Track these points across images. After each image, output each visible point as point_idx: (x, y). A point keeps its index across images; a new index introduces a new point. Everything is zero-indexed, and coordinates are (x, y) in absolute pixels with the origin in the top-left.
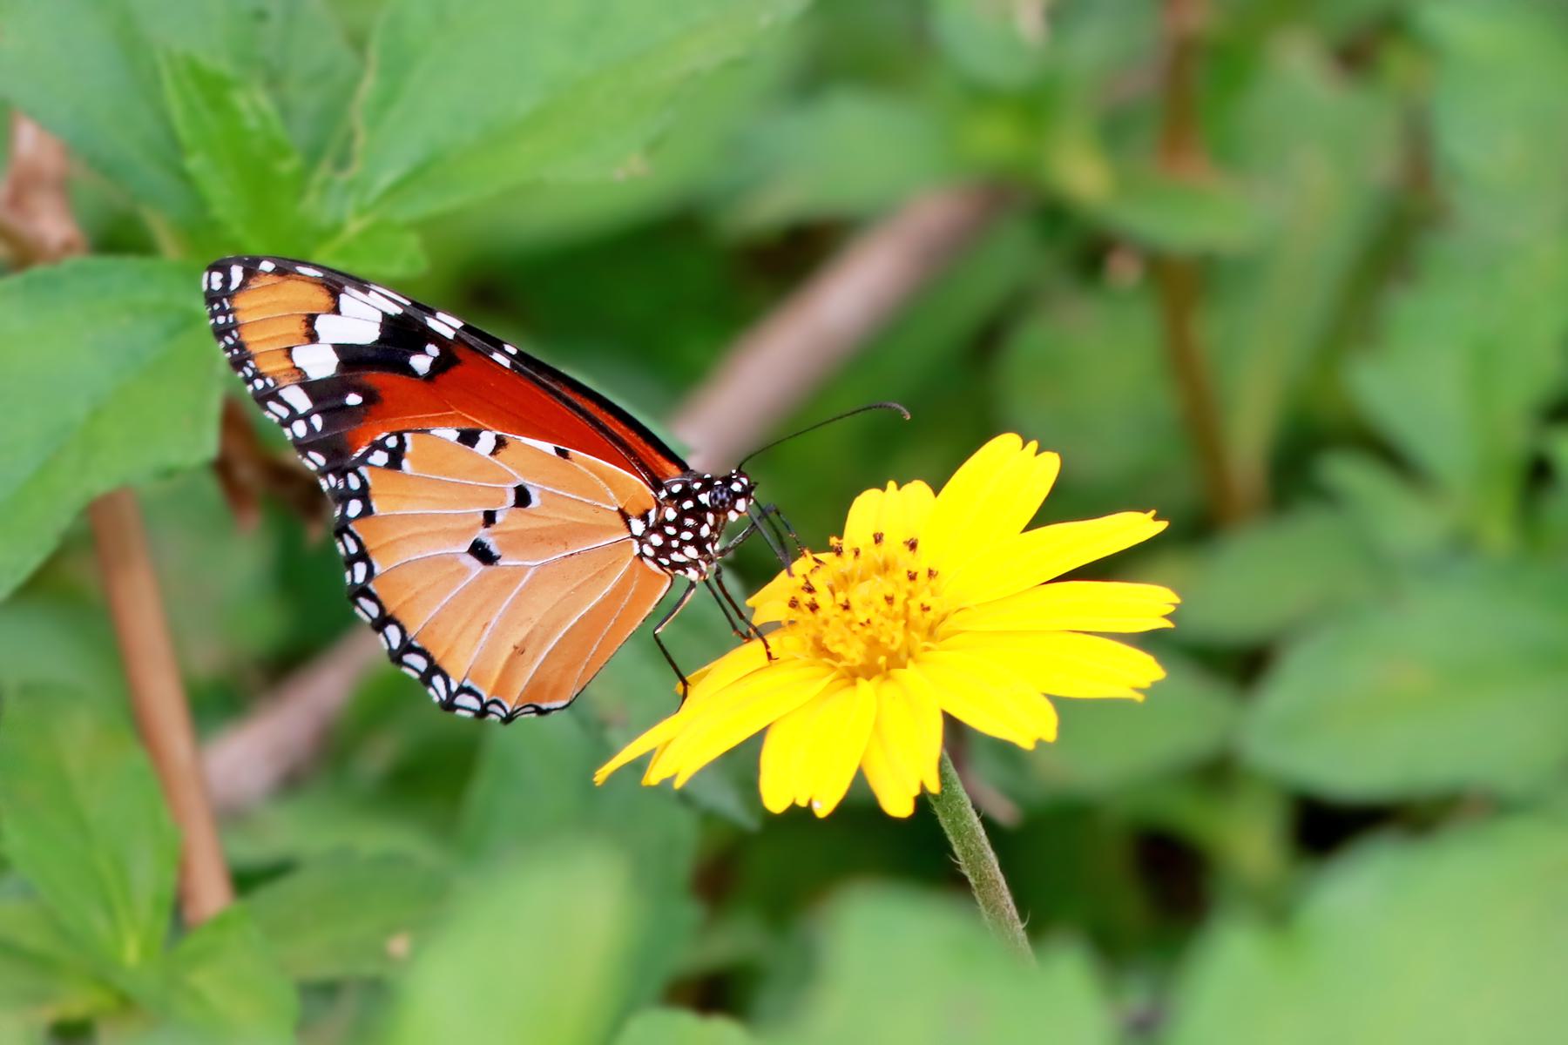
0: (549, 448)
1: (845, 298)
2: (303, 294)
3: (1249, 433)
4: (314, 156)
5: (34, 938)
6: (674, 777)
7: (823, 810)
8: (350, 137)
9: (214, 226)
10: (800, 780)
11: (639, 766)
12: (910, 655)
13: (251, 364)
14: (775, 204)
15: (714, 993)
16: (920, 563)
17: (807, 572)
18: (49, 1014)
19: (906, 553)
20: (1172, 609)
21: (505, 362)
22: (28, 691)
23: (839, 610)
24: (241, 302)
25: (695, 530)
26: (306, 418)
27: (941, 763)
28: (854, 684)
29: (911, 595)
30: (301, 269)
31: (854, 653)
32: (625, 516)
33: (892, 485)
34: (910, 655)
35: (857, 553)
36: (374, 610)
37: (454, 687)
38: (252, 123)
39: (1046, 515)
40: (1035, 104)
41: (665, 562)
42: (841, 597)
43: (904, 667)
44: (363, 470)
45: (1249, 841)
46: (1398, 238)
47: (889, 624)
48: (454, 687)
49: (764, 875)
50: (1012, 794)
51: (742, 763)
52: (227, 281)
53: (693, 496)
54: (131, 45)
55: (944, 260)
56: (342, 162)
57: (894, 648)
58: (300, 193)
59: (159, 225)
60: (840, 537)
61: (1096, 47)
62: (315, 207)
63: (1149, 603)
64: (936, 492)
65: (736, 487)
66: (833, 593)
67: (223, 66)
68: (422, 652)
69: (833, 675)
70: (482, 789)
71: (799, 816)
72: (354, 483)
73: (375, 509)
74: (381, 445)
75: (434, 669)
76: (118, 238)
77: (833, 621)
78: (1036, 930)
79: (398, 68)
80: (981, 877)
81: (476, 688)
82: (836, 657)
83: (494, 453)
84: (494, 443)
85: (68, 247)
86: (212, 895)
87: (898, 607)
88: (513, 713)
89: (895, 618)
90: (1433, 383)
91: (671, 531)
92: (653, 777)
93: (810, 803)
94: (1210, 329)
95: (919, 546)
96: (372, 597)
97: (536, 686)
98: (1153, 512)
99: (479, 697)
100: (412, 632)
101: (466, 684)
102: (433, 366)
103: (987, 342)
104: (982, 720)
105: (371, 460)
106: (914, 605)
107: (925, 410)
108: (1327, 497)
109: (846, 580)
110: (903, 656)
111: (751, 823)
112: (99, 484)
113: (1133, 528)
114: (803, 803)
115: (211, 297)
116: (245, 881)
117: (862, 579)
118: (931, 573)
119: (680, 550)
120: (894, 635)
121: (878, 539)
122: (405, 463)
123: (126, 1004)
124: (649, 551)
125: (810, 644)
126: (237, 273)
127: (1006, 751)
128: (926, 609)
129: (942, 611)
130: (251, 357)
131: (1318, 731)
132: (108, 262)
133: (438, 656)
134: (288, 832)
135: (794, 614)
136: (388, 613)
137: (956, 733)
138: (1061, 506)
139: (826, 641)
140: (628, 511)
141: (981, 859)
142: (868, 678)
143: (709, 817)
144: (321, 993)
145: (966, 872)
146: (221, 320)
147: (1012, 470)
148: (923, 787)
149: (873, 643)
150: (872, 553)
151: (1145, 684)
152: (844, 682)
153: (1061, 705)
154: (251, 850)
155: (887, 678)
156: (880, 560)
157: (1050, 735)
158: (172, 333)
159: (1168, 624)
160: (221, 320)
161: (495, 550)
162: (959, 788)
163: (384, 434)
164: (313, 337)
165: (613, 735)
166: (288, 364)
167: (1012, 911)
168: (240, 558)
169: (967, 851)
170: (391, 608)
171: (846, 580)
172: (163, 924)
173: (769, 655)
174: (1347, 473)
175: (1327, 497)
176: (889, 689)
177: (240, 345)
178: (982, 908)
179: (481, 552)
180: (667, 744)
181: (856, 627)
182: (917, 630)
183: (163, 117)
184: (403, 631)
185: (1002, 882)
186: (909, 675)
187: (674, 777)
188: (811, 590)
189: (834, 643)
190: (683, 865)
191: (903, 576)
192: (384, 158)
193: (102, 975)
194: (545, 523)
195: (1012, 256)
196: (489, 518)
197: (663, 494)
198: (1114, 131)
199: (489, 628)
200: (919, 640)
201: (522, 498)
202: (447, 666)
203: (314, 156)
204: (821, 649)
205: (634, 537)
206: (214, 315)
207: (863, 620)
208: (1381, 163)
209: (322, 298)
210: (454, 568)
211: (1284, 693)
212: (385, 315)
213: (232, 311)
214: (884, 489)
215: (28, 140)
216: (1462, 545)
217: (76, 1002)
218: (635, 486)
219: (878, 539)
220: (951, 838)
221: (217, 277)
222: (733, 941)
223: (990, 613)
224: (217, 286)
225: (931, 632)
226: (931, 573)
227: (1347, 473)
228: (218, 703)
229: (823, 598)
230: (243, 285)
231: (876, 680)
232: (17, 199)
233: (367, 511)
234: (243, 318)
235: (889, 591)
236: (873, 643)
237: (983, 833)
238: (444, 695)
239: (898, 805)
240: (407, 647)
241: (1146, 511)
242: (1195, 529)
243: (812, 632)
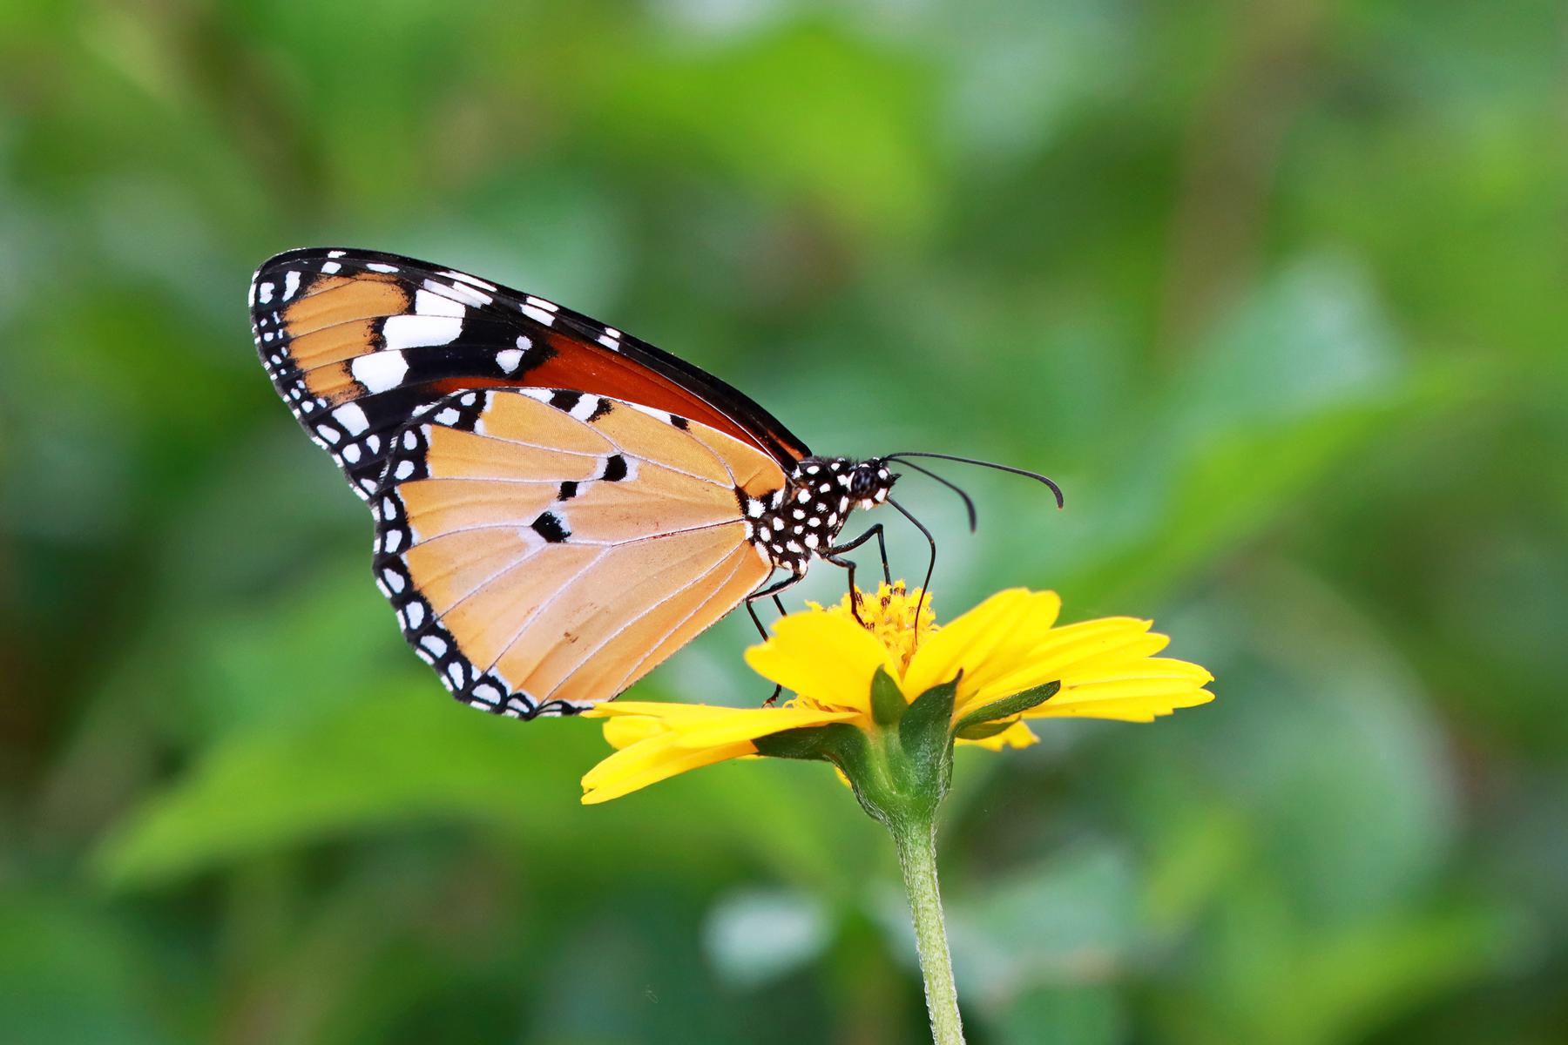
0: (665, 416)
2: (372, 292)
13: (301, 384)
21: (614, 346)
24: (293, 314)
25: (823, 517)
26: (361, 440)
30: (371, 266)
32: (742, 496)
36: (398, 583)
37: (476, 676)
41: (779, 549)
44: (426, 429)
48: (476, 676)
52: (279, 291)
53: (830, 477)
68: (445, 636)
72: (410, 442)
73: (430, 472)
74: (455, 404)
75: (454, 654)
81: (501, 679)
83: (593, 418)
84: (595, 407)
88: (541, 707)
96: (401, 569)
97: (575, 684)
99: (502, 689)
100: (437, 611)
101: (490, 674)
102: (523, 360)
105: (439, 418)
115: (260, 311)
122: (479, 425)
124: (765, 534)
126: (293, 280)
130: (301, 375)
133: (460, 638)
136: (416, 588)
140: (748, 491)
146: (269, 337)
160: (269, 337)
161: (565, 526)
163: (378, 543)
164: (378, 344)
166: (346, 380)
170: (420, 581)
177: (289, 364)
179: (548, 528)
184: (428, 610)
194: (639, 500)
196: (568, 490)
197: (797, 474)
199: (535, 613)
201: (616, 469)
202: (468, 653)
205: (750, 519)
206: (261, 332)
209: (396, 297)
210: (511, 543)
212: (469, 308)
213: (284, 325)
218: (764, 469)
221: (267, 289)
224: (266, 297)
230: (299, 294)
233: (420, 474)
234: (293, 331)
238: (460, 684)
240: (430, 627)
241: (1145, 618)
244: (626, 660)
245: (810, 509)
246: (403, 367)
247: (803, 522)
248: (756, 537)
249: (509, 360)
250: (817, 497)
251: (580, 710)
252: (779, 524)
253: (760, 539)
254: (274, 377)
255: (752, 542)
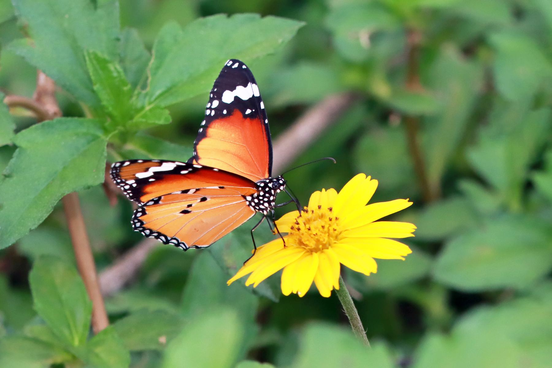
1: (305, 130)
3: (435, 172)
4: (135, 85)
5: (45, 337)
6: (253, 284)
7: (301, 295)
8: (147, 78)
9: (103, 107)
10: (295, 285)
11: (242, 281)
12: (330, 245)
14: (283, 99)
15: (262, 354)
16: (333, 215)
17: (296, 218)
18: (50, 362)
19: (328, 212)
20: (414, 230)
22: (42, 257)
23: (307, 230)
25: (269, 198)
27: (340, 279)
28: (312, 254)
29: (330, 226)
31: (312, 244)
33: (324, 190)
34: (330, 245)
35: (313, 212)
38: (115, 74)
39: (372, 201)
40: (366, 67)
41: (258, 208)
42: (308, 226)
43: (328, 248)
45: (436, 305)
46: (482, 112)
47: (323, 234)
49: (281, 316)
50: (360, 291)
51: (275, 281)
54: (76, 49)
55: (336, 118)
56: (144, 87)
57: (324, 242)
58: (131, 97)
59: (85, 107)
60: (307, 206)
61: (385, 49)
62: (136, 102)
63: (406, 229)
64: (338, 192)
65: (281, 182)
66: (305, 225)
67: (106, 57)
69: (305, 251)
70: (189, 288)
71: (294, 296)
76: (71, 111)
77: (305, 234)
78: (371, 336)
79: (162, 57)
80: (352, 317)
82: (306, 245)
85: (55, 114)
86: (102, 323)
87: (326, 229)
89: (325, 233)
90: (497, 157)
91: (261, 198)
92: (247, 284)
93: (297, 292)
94: (423, 139)
95: (333, 210)
98: (408, 199)
103: (350, 143)
104: (354, 266)
106: (331, 228)
107: (333, 165)
108: (460, 193)
109: (308, 221)
110: (327, 245)
111: (277, 300)
112: (66, 190)
113: (403, 204)
114: (295, 292)
116: (113, 318)
117: (314, 220)
118: (337, 219)
119: (263, 204)
120: (325, 238)
121: (319, 207)
123: (74, 358)
124: (253, 204)
125: (297, 241)
127: (358, 276)
128: (335, 230)
129: (340, 231)
131: (463, 269)
132: (69, 119)
134: (126, 302)
135: (293, 231)
137: (343, 269)
138: (379, 197)
139: (303, 240)
141: (353, 313)
142: (316, 252)
143: (262, 298)
144: (137, 355)
145: (347, 315)
147: (362, 185)
148: (334, 287)
149: (318, 241)
150: (318, 212)
151: (405, 255)
152: (308, 253)
153: (379, 262)
154: (115, 308)
155: (322, 252)
156: (320, 214)
157: (375, 271)
158: (89, 142)
159: (413, 235)
162: (345, 288)
165: (231, 271)
167: (362, 328)
168: (110, 214)
169: (347, 308)
171: (308, 221)
172: (87, 333)
173: (285, 245)
174: (468, 186)
175: (460, 193)
176: (323, 256)
178: (352, 326)
180: (250, 274)
181: (312, 236)
182: (332, 237)
183: (87, 73)
185: (359, 318)
186: (329, 251)
187: (253, 284)
188: (298, 224)
189: (305, 241)
190: (253, 313)
191: (327, 220)
192: (157, 85)
193: (67, 350)
195: (358, 116)
198: (392, 75)
200: (332, 240)
203: (135, 85)
204: (301, 243)
207: (315, 233)
208: (478, 86)
211: (448, 257)
214: (321, 191)
215: (42, 79)
216: (504, 209)
217: (59, 358)
219: (319, 207)
220: (342, 304)
222: (270, 337)
223: (357, 232)
225: (336, 238)
226: (337, 219)
227: (468, 186)
228: (104, 260)
229: (302, 226)
231: (318, 253)
232: (39, 99)
235: (323, 224)
236: (318, 241)
237: (353, 302)
239: (326, 293)
241: (406, 199)
242: (420, 204)
243: (298, 237)
244: (213, 236)
245: (264, 196)
246: (233, 100)
247: (262, 200)
248: (250, 204)
249: (248, 111)
250: (265, 193)
251: (201, 247)
252: (256, 201)
253: (251, 205)
254: (128, 196)
255: (249, 205)
